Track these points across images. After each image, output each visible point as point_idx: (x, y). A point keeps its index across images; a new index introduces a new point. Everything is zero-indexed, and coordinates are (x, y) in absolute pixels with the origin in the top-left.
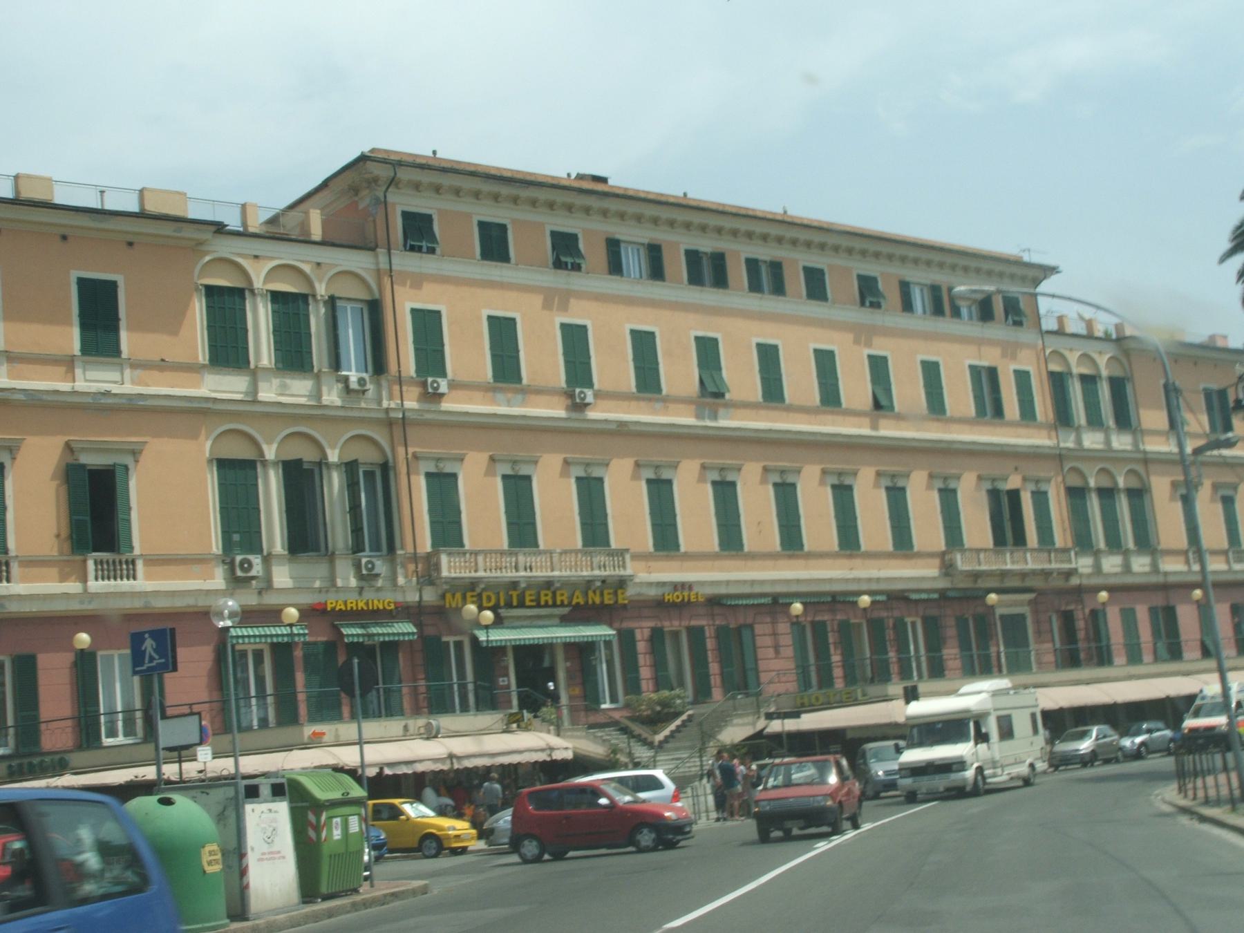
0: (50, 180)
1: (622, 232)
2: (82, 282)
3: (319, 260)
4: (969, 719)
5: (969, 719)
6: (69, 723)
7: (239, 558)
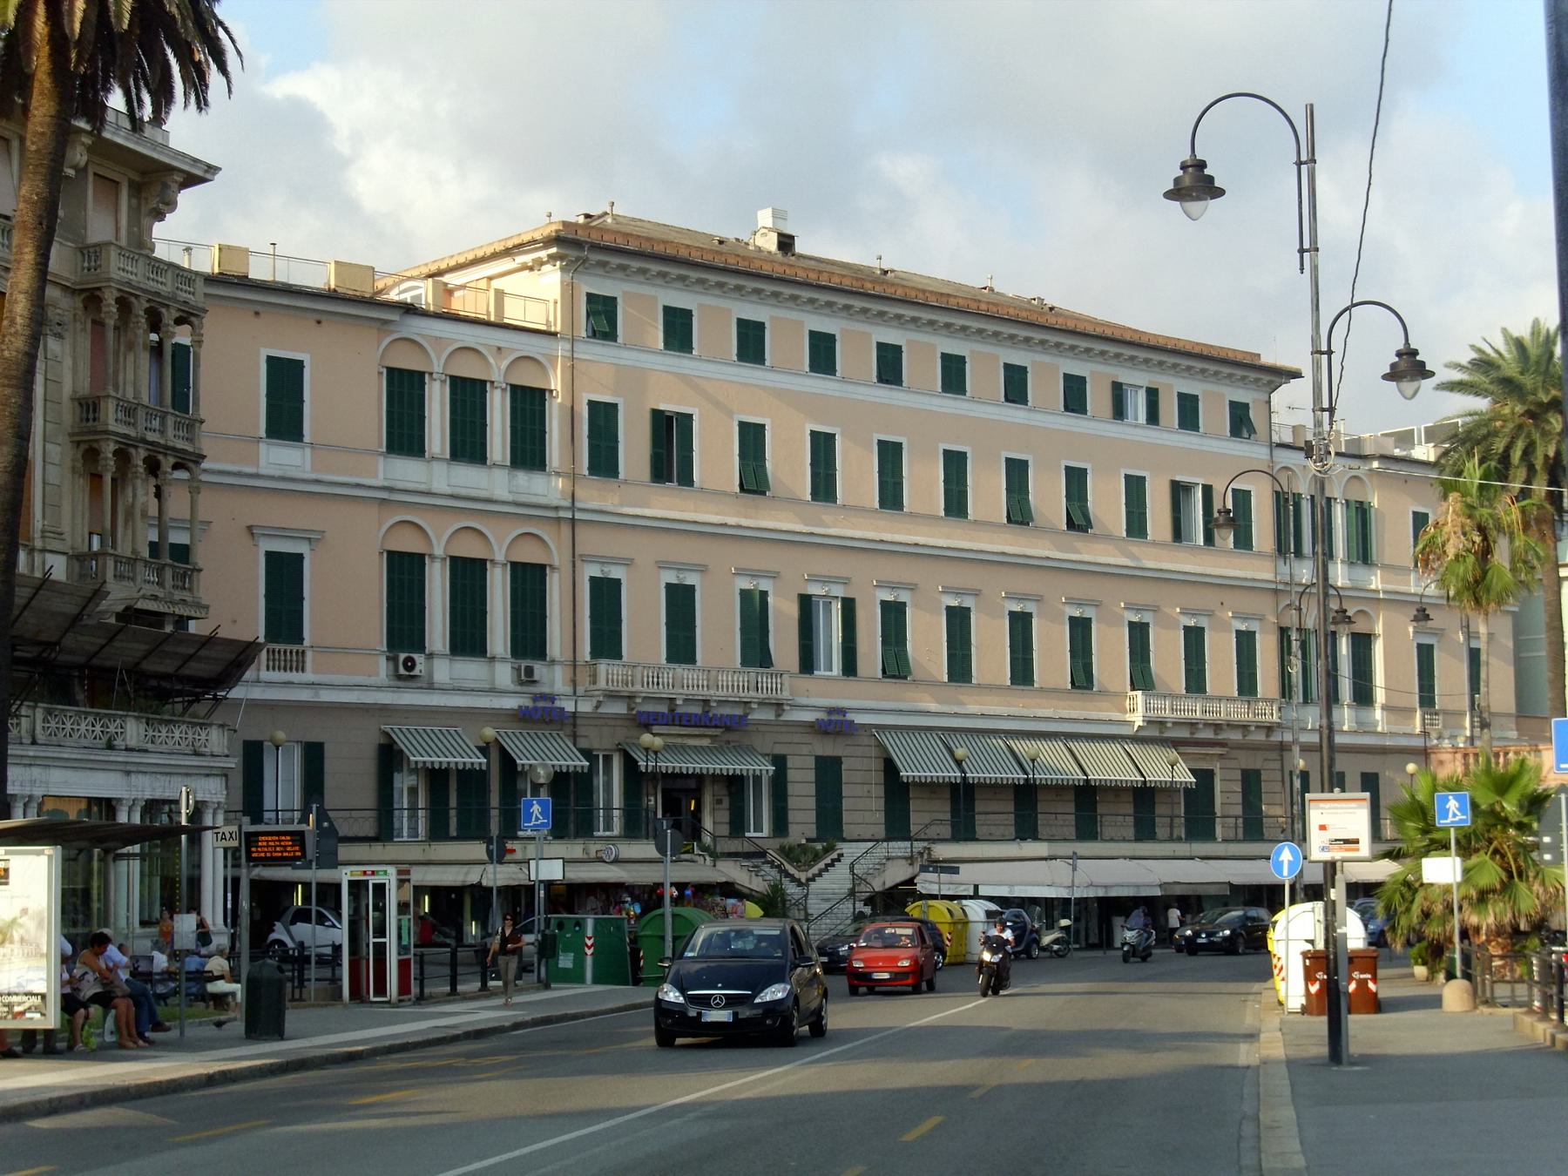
0: (247, 250)
1: (1126, 376)
2: (270, 359)
3: (502, 345)
4: (297, 884)
5: (297, 884)
6: (373, 814)
7: (402, 656)
